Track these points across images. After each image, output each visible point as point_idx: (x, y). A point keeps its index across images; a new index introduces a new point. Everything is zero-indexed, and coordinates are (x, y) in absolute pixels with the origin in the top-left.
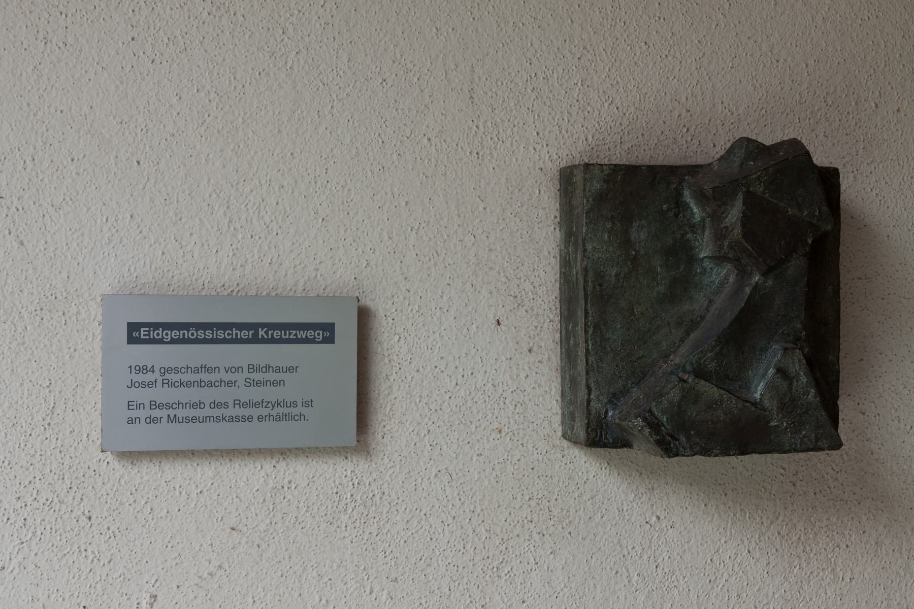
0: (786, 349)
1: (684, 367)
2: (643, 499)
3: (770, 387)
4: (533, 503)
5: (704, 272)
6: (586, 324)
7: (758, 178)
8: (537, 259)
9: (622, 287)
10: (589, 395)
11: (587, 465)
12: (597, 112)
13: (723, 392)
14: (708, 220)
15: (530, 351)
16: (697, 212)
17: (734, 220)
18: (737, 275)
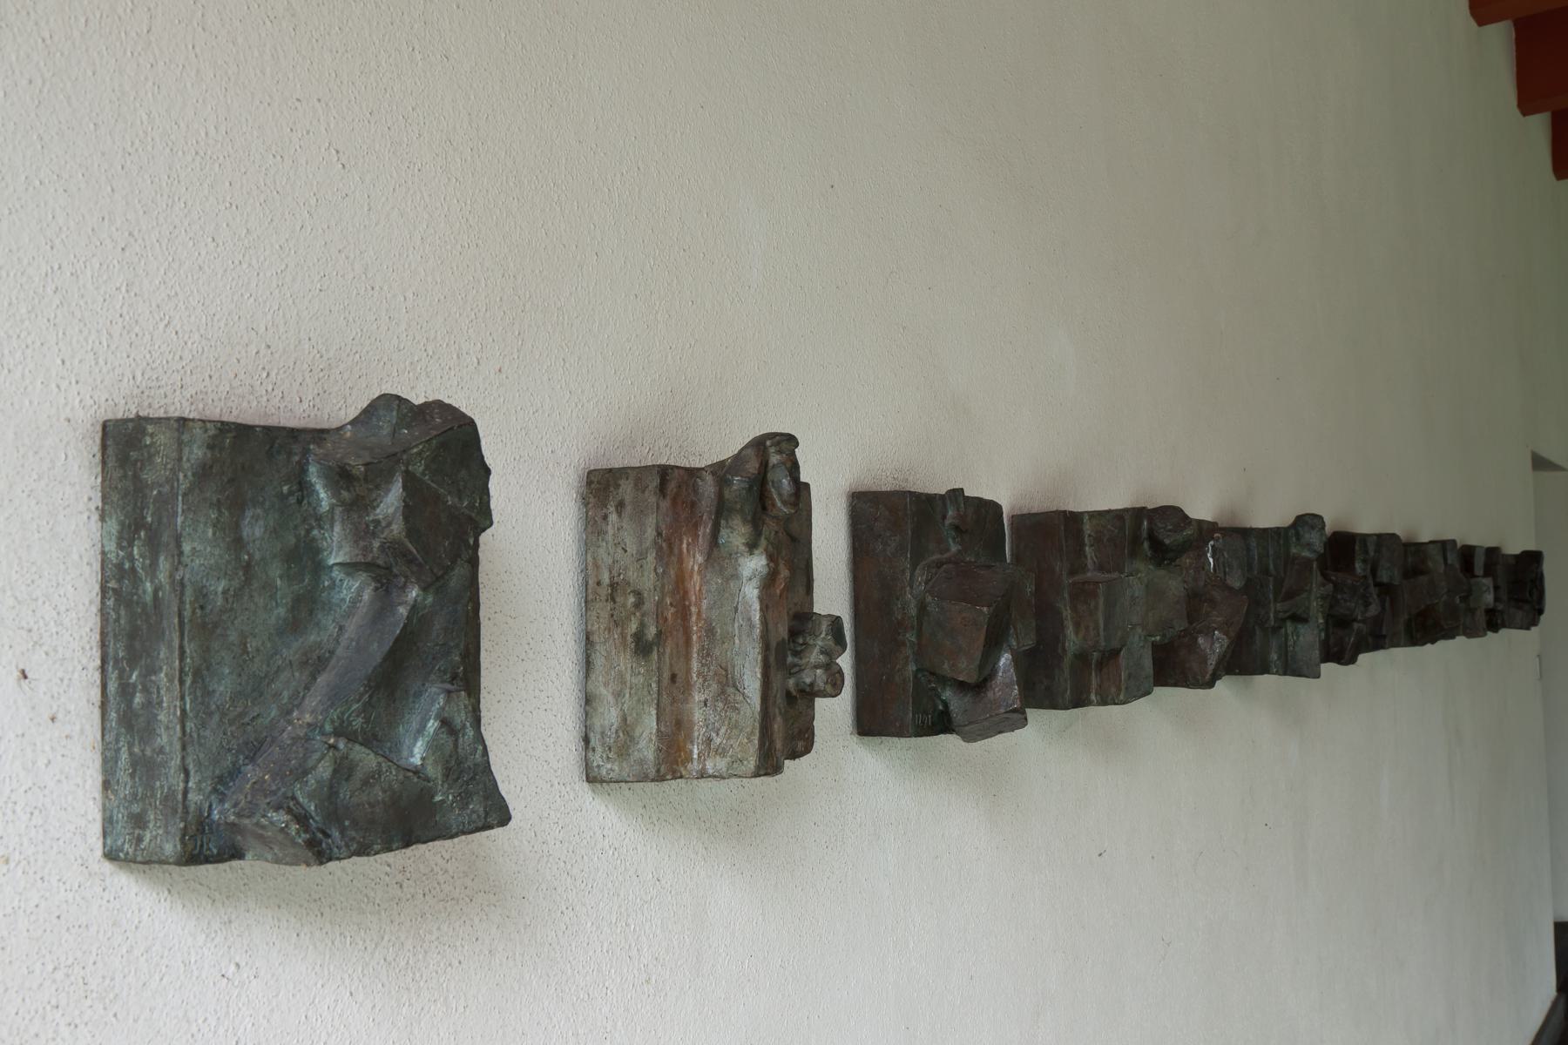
0: (449, 692)
1: (322, 727)
2: (217, 940)
3: (434, 746)
4: (59, 975)
5: (333, 585)
6: (181, 670)
7: (419, 454)
8: (62, 567)
9: (232, 609)
10: (187, 781)
11: (139, 899)
12: (148, 337)
13: (381, 759)
14: (338, 510)
15: (53, 719)
16: (324, 497)
17: (391, 511)
18: (376, 589)
